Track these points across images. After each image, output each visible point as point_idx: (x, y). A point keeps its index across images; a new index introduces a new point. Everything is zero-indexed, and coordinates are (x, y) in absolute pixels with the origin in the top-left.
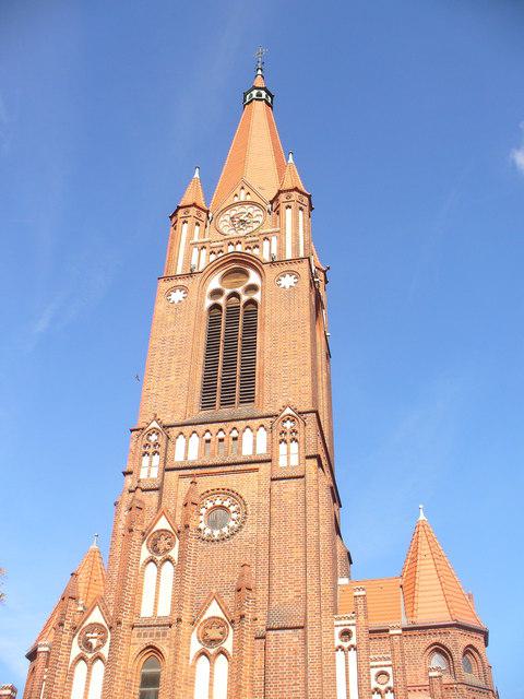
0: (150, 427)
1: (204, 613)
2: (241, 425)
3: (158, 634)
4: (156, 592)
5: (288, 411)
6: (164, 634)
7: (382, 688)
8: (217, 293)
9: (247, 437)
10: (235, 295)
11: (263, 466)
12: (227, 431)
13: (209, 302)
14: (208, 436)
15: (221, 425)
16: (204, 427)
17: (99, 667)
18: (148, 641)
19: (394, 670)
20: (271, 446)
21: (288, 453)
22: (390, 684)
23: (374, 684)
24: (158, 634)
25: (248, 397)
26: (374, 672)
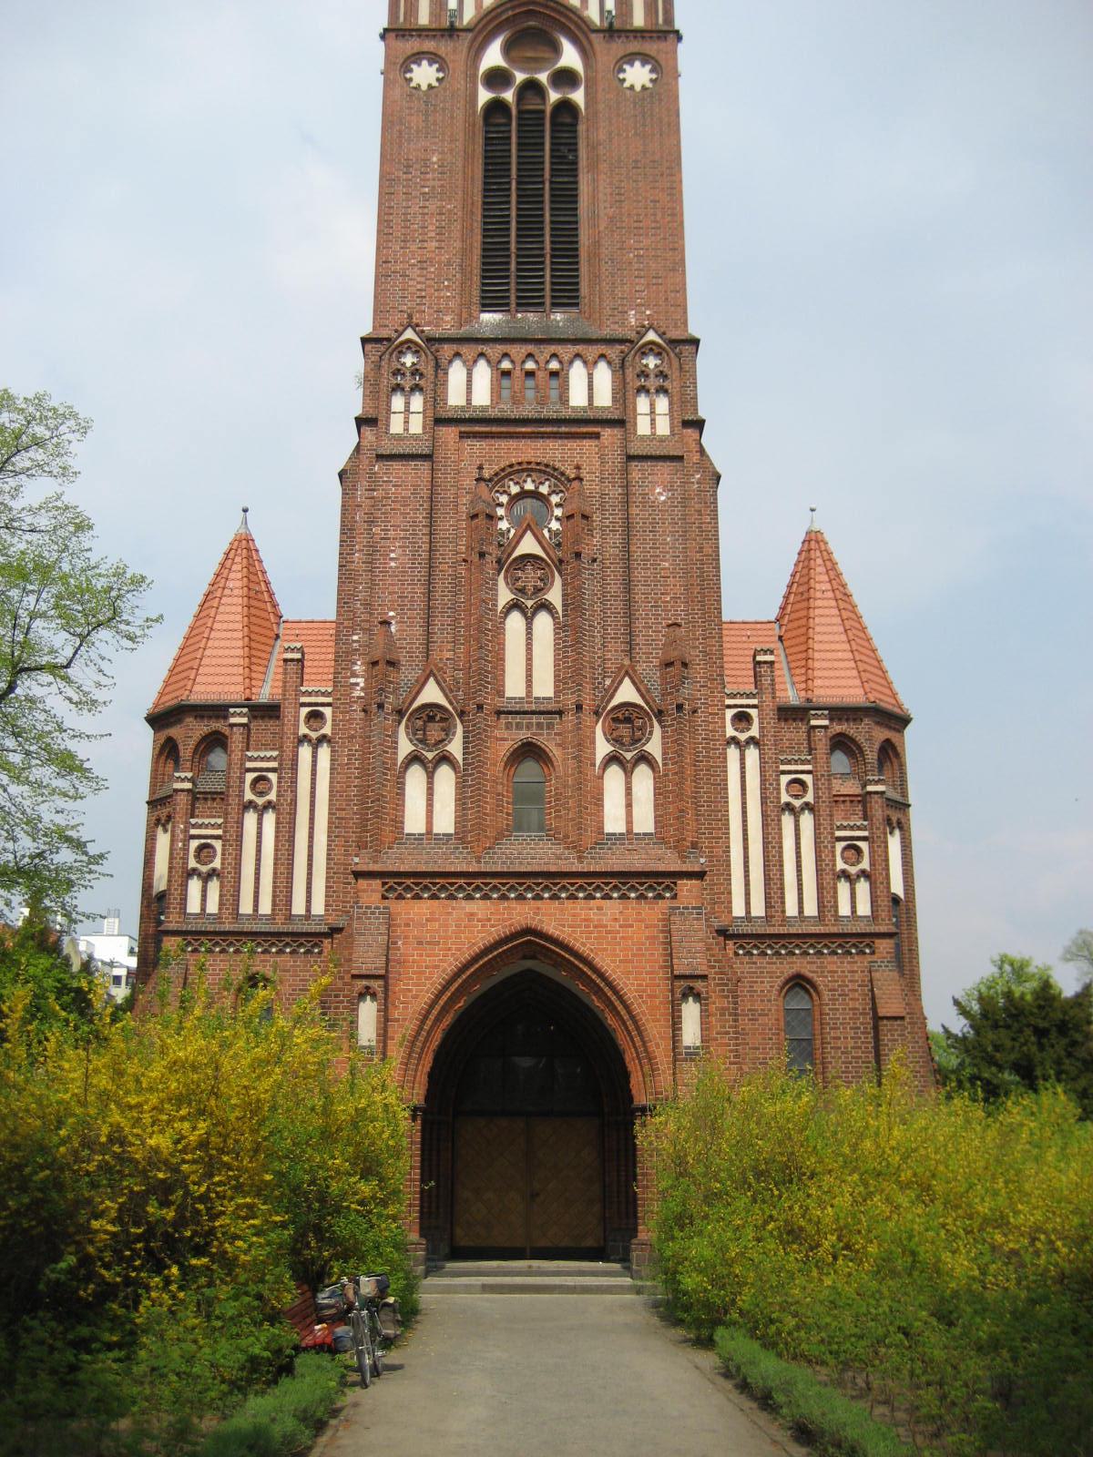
0: (403, 338)
1: (612, 696)
2: (566, 351)
3: (539, 725)
4: (530, 659)
5: (651, 336)
6: (550, 726)
7: (797, 803)
8: (497, 78)
9: (577, 373)
10: (532, 87)
11: (607, 433)
12: (541, 359)
13: (484, 96)
14: (506, 365)
15: (530, 348)
16: (500, 348)
17: (445, 776)
18: (524, 735)
19: (816, 780)
20: (623, 394)
21: (652, 412)
22: (809, 798)
23: (785, 798)
24: (539, 725)
25: (567, 295)
26: (785, 779)
